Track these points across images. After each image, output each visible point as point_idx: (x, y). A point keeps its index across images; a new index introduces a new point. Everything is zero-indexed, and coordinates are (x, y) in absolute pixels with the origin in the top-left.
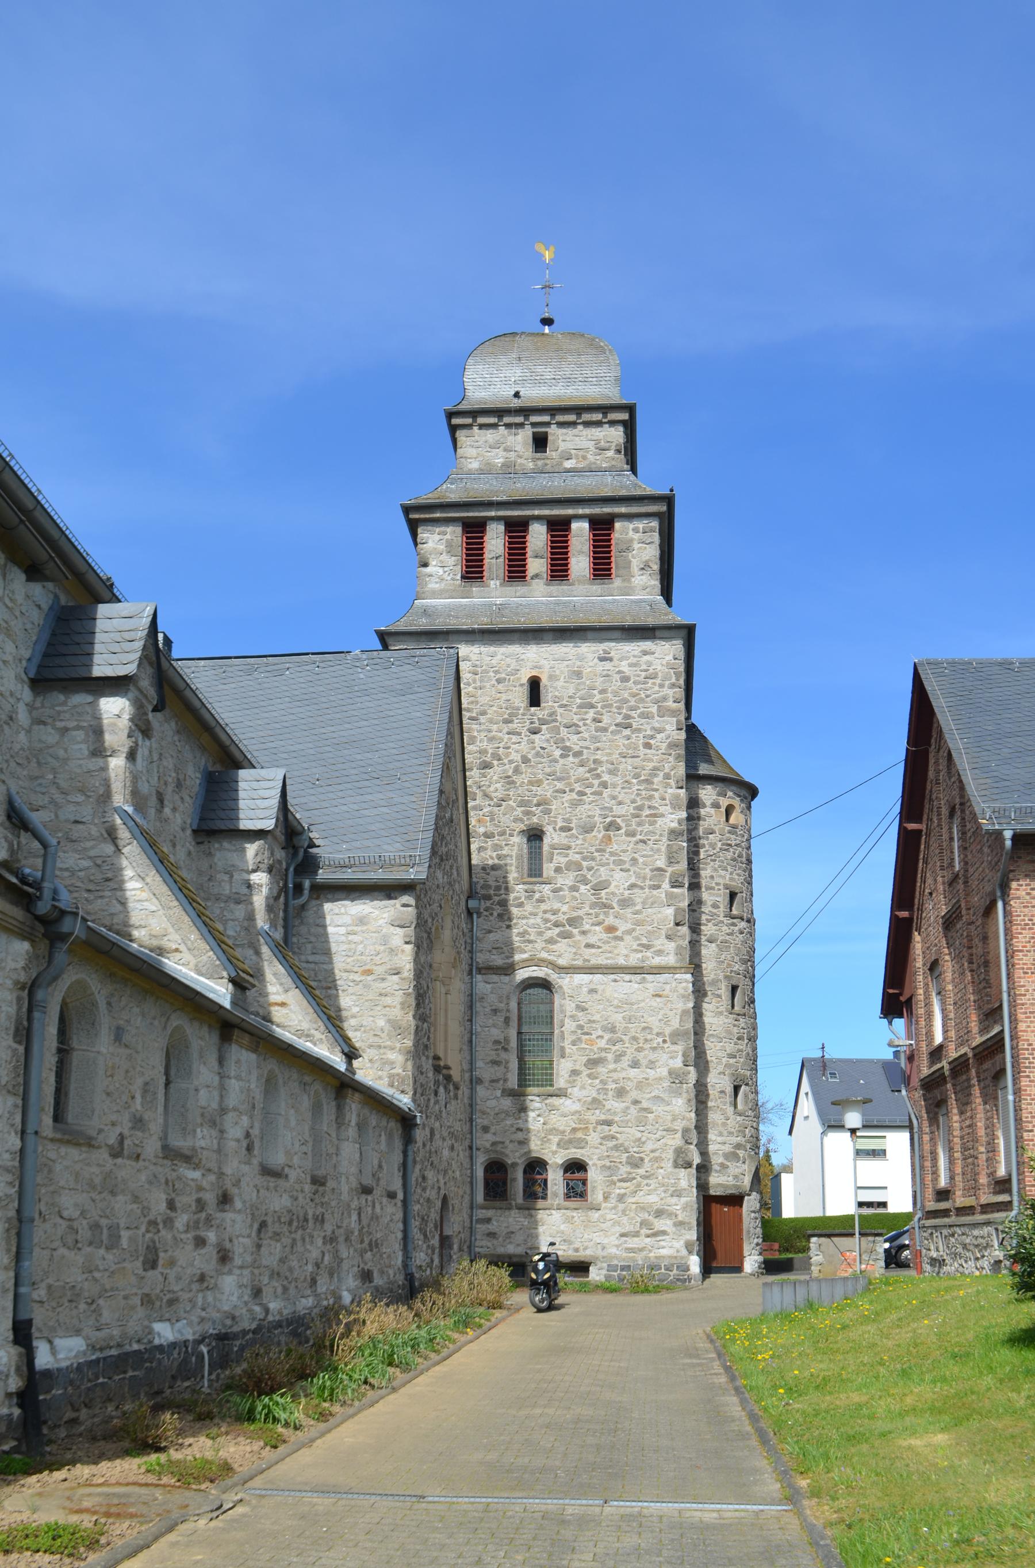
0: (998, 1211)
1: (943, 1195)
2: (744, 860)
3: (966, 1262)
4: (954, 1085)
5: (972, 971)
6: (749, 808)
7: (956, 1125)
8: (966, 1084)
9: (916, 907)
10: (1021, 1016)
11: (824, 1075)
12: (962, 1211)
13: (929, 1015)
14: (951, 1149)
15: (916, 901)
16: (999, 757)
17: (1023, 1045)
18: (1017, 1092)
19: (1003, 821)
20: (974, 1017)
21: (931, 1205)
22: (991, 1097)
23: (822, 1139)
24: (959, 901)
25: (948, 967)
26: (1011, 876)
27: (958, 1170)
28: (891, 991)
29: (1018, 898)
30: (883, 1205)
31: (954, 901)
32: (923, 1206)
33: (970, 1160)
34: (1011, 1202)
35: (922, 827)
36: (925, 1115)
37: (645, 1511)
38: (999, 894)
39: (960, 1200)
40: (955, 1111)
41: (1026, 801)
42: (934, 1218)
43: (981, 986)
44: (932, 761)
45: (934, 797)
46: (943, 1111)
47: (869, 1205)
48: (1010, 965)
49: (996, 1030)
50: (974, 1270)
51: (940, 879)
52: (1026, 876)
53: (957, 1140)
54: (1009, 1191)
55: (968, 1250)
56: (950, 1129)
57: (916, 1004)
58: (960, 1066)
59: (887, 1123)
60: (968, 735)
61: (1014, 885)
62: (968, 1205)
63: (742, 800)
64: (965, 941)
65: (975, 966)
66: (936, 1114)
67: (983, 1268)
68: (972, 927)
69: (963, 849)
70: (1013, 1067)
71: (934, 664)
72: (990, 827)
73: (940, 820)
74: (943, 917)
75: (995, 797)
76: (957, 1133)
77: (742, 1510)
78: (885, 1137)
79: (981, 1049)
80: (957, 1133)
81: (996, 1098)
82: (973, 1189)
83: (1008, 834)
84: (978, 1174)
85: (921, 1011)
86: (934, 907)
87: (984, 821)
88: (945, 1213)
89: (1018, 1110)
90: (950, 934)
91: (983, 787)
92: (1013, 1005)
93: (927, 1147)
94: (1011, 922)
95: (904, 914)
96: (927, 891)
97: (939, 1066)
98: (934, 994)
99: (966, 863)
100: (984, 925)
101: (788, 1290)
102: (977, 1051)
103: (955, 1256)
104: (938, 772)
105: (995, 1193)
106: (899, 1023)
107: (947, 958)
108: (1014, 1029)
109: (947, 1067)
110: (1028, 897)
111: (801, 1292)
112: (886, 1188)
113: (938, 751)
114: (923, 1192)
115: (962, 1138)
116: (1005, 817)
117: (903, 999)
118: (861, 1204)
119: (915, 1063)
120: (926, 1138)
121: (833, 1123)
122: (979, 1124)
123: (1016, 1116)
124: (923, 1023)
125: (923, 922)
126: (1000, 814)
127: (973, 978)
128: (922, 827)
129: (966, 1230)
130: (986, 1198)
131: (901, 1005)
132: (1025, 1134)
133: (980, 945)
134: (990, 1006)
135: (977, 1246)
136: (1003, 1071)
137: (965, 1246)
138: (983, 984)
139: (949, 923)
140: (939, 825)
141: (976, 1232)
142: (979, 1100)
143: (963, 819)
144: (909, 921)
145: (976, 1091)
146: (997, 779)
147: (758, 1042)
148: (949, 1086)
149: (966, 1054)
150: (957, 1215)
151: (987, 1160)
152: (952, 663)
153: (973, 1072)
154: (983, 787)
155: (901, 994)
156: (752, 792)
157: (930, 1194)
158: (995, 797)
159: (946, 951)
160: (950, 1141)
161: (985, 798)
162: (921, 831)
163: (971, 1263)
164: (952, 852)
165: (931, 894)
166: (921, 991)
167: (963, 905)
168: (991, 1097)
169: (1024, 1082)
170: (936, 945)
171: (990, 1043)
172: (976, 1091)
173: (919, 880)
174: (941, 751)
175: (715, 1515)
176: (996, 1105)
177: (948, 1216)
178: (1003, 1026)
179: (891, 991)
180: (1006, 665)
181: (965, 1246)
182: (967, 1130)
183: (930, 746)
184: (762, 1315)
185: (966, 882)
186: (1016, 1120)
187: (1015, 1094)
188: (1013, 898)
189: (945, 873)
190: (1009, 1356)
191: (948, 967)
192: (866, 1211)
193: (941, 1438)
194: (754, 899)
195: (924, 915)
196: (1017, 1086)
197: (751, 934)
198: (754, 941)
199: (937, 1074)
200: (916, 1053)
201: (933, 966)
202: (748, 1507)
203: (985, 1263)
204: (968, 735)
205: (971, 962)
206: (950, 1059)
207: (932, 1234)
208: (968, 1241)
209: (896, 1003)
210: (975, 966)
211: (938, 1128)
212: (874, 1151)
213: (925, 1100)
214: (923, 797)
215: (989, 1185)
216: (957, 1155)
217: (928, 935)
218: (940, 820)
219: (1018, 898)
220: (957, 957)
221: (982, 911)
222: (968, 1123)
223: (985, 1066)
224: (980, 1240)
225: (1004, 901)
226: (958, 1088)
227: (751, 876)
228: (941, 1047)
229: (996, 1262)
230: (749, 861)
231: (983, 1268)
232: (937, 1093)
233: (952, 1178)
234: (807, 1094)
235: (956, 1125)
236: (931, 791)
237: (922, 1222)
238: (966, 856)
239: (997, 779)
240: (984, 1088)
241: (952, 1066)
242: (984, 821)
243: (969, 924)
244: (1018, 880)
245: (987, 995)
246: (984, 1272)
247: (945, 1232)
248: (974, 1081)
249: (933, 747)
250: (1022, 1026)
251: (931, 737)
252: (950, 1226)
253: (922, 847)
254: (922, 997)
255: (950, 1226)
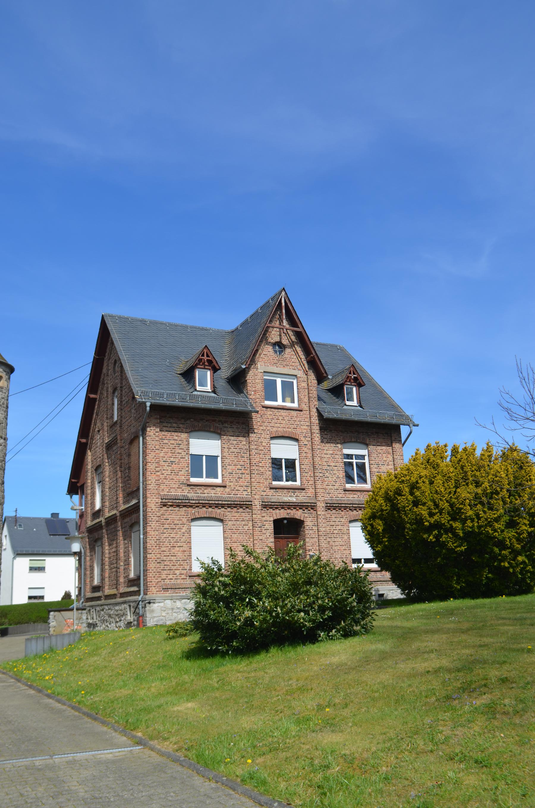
0: (130, 596)
1: (96, 589)
2: (5, 406)
3: (110, 624)
4: (107, 530)
5: (121, 471)
6: (9, 378)
7: (107, 551)
8: (114, 530)
9: (90, 437)
10: (148, 495)
11: (15, 526)
12: (108, 597)
13: (93, 494)
14: (103, 564)
15: (90, 434)
16: (142, 366)
17: (149, 510)
18: (145, 533)
19: (146, 397)
20: (121, 495)
21: (89, 595)
22: (127, 537)
23: (13, 561)
24: (116, 435)
25: (107, 469)
26: (147, 425)
27: (107, 575)
28: (73, 480)
29: (150, 436)
30: (42, 597)
31: (114, 435)
32: (85, 595)
33: (114, 570)
34: (139, 591)
35: (97, 397)
36: (88, 547)
37: (76, 758)
38: (141, 433)
39: (107, 591)
40: (107, 544)
41: (155, 389)
42: (91, 601)
43: (126, 479)
44: (105, 364)
45: (105, 382)
46: (99, 543)
47: (35, 597)
48: (145, 469)
49: (134, 502)
50: (115, 628)
51: (105, 424)
52: (154, 425)
53: (107, 559)
54: (139, 585)
55: (112, 618)
56: (103, 553)
57: (87, 488)
58: (111, 521)
59: (47, 553)
60: (128, 354)
61: (148, 429)
62: (113, 593)
63: (6, 374)
64: (119, 456)
65: (123, 469)
66: (94, 546)
67: (120, 627)
68: (123, 449)
69: (120, 409)
70: (143, 521)
71: (111, 316)
72: (140, 400)
73: (107, 394)
74: (106, 444)
75: (142, 385)
76: (107, 556)
77: (122, 751)
78: (45, 560)
79: (124, 511)
80: (107, 556)
81: (131, 537)
82: (116, 585)
83: (148, 404)
84: (119, 577)
85: (89, 492)
86: (100, 438)
87: (137, 397)
88: (98, 598)
89: (145, 543)
90: (109, 452)
91: (136, 380)
92: (145, 489)
93: (88, 564)
94: (146, 448)
95: (84, 441)
96: (97, 429)
97: (98, 520)
98: (96, 483)
99: (121, 417)
100: (129, 448)
101: (40, 642)
102: (122, 513)
103: (103, 621)
104: (108, 370)
105: (128, 586)
106: (76, 498)
107: (107, 464)
108: (145, 501)
109: (103, 521)
110: (154, 436)
111: (47, 642)
112: (44, 588)
113: (109, 360)
114: (85, 587)
115: (110, 558)
116: (146, 395)
117: (79, 485)
118: (30, 598)
119: (84, 519)
120: (88, 558)
121: (19, 552)
122: (121, 551)
123: (144, 546)
124: (89, 498)
125: (93, 445)
126: (145, 394)
127: (121, 475)
128: (97, 397)
129: (111, 607)
130: (123, 589)
131: (78, 488)
132: (148, 555)
133: (127, 458)
134: (131, 490)
135: (117, 615)
136: (138, 523)
137: (110, 616)
138: (127, 478)
139: (109, 447)
140: (107, 397)
141: (117, 608)
142: (121, 538)
143: (121, 394)
144: (86, 444)
145: (120, 534)
146: (142, 377)
147: (4, 506)
148: (104, 531)
149: (115, 514)
150: (105, 599)
151: (124, 570)
152: (120, 317)
153: (119, 523)
154: (136, 380)
155: (78, 482)
156: (10, 370)
157: (88, 588)
158: (142, 385)
159: (107, 461)
160: (102, 560)
161: (137, 386)
162: (96, 399)
163: (113, 625)
164: (113, 411)
165: (99, 431)
166: (89, 481)
167: (119, 437)
168: (127, 537)
169: (149, 529)
170: (100, 458)
171: (130, 509)
172: (120, 534)
173: (93, 424)
174: (111, 360)
175: (111, 755)
176: (131, 541)
177: (101, 600)
178: (139, 500)
179: (73, 480)
180: (143, 322)
181: (110, 616)
182: (113, 554)
183: (105, 356)
184: (26, 657)
185: (121, 426)
186: (144, 548)
187: (144, 534)
188: (148, 436)
189: (108, 421)
190: (187, 664)
191: (107, 469)
192: (33, 601)
193: (190, 705)
194: (8, 427)
195: (94, 442)
196: (145, 531)
197: (5, 446)
198: (6, 450)
199: (98, 525)
200: (85, 513)
201: (98, 468)
202: (126, 749)
203: (122, 624)
204: (128, 354)
205: (121, 467)
206: (106, 517)
207: (90, 610)
208: (112, 613)
209: (75, 487)
210: (123, 469)
211: (95, 553)
212: (39, 567)
213: (88, 538)
214: (99, 382)
215: (125, 582)
216: (107, 567)
217: (95, 452)
218: (107, 394)
219: (150, 436)
220: (113, 464)
221: (129, 441)
222: (113, 550)
223: (126, 520)
224: (119, 612)
225: (143, 437)
226: (109, 532)
227: (7, 415)
228: (99, 511)
229: (128, 623)
230: (7, 407)
231: (120, 627)
232: (96, 535)
233: (102, 579)
234: (6, 536)
235: (107, 551)
236: (103, 379)
237: (84, 604)
238: (122, 413)
239: (142, 377)
240: (124, 532)
241: (107, 520)
242: (137, 397)
243: (121, 448)
244: (150, 427)
245: (129, 484)
246: (121, 629)
247: (98, 609)
248: (120, 528)
249: (107, 357)
250: (149, 500)
251: (105, 352)
252: (101, 605)
253: (96, 407)
254: (89, 484)
255: (101, 605)
